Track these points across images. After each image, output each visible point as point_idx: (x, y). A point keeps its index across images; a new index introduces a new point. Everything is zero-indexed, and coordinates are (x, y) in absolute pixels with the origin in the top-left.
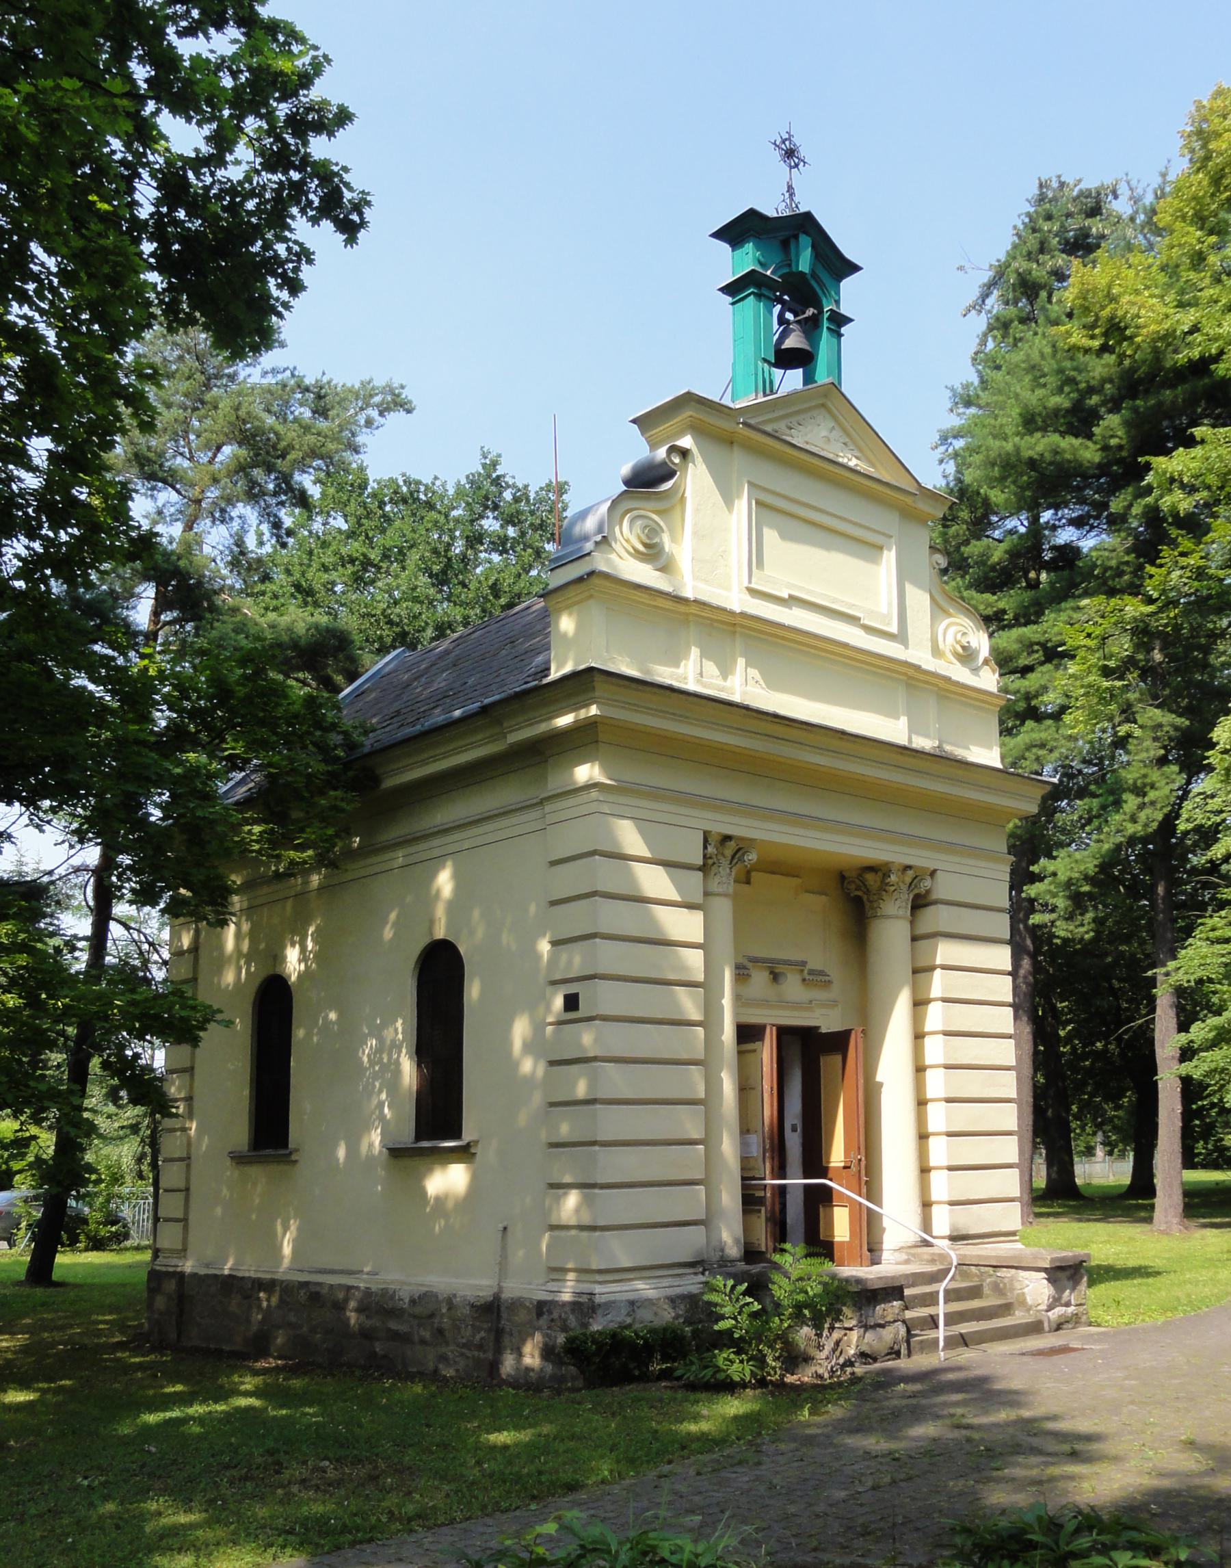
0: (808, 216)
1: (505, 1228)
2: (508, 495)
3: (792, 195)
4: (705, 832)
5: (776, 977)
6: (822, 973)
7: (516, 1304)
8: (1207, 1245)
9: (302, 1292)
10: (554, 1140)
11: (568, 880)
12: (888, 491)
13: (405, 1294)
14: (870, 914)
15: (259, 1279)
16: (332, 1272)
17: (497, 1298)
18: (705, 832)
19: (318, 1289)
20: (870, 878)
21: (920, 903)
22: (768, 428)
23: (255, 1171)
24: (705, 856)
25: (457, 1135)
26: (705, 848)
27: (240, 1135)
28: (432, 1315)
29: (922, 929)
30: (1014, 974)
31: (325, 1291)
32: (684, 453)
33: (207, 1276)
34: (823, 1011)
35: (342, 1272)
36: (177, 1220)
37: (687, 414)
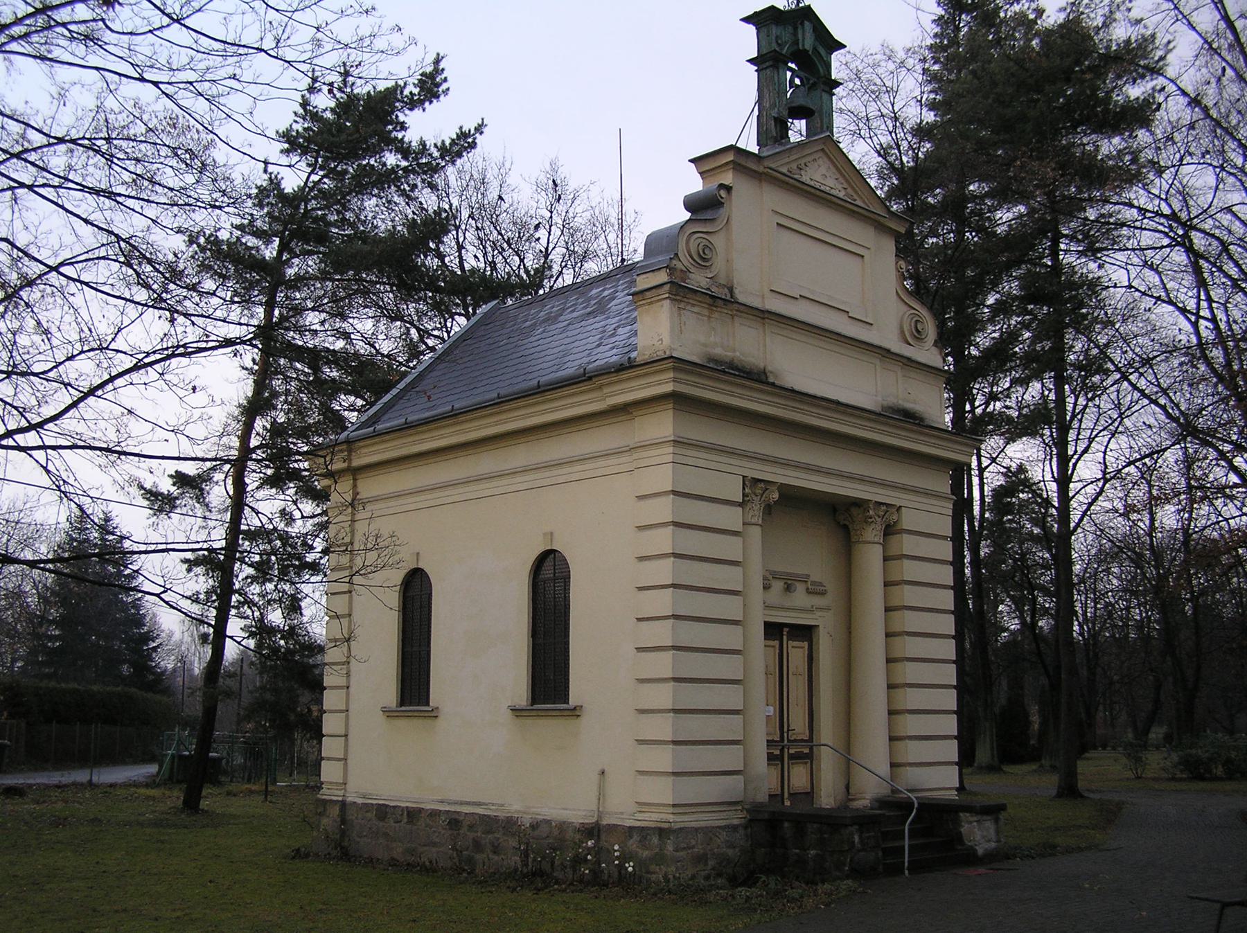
0: (808, 9)
5: (788, 588)
6: (821, 584)
8: (166, 279)
10: (640, 707)
17: (597, 823)
20: (854, 511)
21: (890, 530)
22: (784, 170)
23: (402, 723)
24: (744, 495)
27: (390, 695)
29: (893, 551)
32: (728, 189)
34: (820, 614)
36: (339, 760)
37: (730, 157)
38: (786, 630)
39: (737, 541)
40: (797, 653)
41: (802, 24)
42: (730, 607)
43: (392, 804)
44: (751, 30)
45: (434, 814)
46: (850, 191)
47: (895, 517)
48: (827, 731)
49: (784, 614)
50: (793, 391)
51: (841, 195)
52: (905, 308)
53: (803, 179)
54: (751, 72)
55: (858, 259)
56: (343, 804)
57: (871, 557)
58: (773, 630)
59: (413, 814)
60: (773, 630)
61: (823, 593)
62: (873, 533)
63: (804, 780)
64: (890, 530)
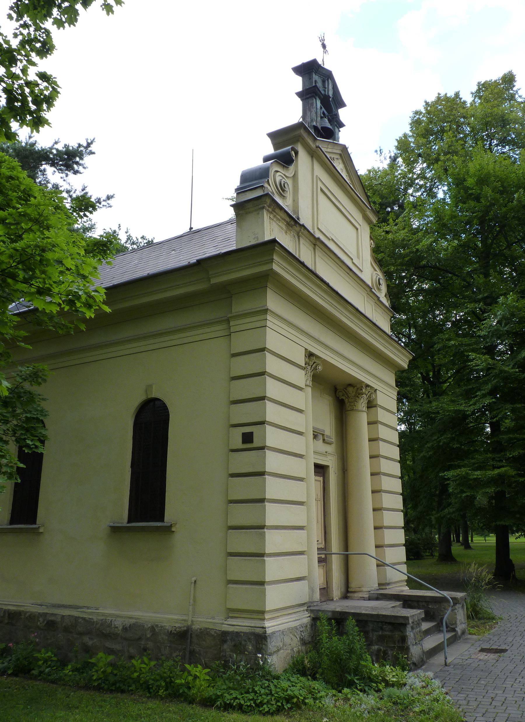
1: (195, 581)
2: (50, 186)
7: (204, 633)
11: (243, 365)
12: (361, 202)
13: (118, 623)
15: (9, 610)
18: (306, 349)
19: (53, 618)
20: (350, 389)
25: (161, 518)
28: (140, 639)
30: (401, 478)
31: (59, 619)
41: (328, 80)
45: (32, 617)
52: (373, 270)
57: (361, 419)
61: (330, 444)
62: (362, 404)
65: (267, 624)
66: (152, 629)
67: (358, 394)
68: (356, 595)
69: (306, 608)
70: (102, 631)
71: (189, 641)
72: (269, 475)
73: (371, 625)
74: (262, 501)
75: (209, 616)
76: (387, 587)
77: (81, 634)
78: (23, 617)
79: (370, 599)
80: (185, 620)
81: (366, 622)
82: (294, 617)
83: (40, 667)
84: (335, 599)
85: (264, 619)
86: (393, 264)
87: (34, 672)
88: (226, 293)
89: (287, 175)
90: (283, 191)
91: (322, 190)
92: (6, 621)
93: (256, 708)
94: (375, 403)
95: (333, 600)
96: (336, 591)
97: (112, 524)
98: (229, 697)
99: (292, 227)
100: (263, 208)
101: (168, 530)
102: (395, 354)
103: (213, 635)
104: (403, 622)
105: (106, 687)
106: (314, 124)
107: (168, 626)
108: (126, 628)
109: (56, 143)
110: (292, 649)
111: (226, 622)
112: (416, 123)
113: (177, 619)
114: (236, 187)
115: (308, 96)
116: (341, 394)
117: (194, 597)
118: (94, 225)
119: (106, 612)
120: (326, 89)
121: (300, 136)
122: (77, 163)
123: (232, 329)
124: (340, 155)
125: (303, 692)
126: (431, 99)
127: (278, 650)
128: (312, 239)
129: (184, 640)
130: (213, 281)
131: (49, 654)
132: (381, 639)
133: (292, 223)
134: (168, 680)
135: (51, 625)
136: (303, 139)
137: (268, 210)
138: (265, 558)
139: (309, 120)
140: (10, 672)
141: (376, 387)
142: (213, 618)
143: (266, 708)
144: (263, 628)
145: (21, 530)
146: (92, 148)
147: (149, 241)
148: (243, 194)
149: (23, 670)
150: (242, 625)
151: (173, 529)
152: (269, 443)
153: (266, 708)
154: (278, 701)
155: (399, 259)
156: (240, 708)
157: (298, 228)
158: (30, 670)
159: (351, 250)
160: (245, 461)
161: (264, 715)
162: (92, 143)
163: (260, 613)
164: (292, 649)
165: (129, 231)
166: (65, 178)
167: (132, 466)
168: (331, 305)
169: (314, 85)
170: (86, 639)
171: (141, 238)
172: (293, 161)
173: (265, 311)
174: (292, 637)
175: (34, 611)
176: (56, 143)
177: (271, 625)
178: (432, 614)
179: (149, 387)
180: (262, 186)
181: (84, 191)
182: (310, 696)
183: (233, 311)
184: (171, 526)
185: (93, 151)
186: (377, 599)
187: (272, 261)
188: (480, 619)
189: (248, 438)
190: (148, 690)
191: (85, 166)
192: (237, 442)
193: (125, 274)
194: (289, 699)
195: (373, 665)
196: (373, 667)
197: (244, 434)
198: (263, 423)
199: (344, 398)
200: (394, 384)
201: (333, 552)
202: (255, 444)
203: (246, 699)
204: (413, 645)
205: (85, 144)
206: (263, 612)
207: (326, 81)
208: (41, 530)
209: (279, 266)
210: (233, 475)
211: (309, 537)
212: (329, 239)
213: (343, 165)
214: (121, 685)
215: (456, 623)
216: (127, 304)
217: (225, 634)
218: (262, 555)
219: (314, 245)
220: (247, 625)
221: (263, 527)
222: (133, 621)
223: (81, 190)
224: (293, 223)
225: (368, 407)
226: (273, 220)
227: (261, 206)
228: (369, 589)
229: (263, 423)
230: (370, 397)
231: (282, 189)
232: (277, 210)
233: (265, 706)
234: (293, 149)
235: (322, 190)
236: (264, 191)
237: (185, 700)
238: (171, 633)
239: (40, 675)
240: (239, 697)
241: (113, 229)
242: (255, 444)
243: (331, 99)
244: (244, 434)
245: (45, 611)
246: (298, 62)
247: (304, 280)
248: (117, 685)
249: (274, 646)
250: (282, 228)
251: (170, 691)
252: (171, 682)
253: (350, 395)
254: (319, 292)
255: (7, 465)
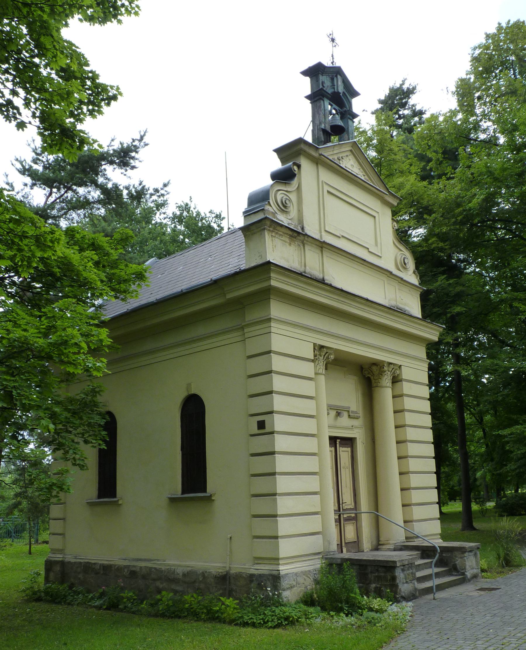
1: (231, 538)
3: (333, 58)
4: (314, 344)
5: (338, 414)
7: (238, 576)
9: (126, 570)
13: (180, 571)
14: (375, 385)
15: (103, 564)
16: (140, 560)
18: (314, 344)
19: (134, 569)
20: (374, 368)
22: (331, 158)
25: (205, 491)
26: (314, 351)
28: (194, 582)
31: (138, 570)
33: (75, 563)
35: (145, 560)
36: (60, 534)
38: (338, 441)
39: (312, 383)
40: (344, 453)
41: (336, 76)
42: (309, 426)
43: (93, 562)
44: (308, 79)
45: (120, 569)
46: (366, 177)
47: (398, 372)
48: (365, 504)
49: (346, 431)
50: (342, 290)
51: (363, 178)
52: (397, 250)
53: (341, 165)
54: (308, 105)
55: (372, 219)
56: (62, 563)
57: (385, 394)
58: (333, 440)
59: (107, 569)
60: (333, 440)
61: (357, 418)
62: (386, 380)
63: (353, 534)
64: (396, 380)
65: (281, 568)
66: (203, 574)
67: (381, 373)
68: (384, 547)
69: (321, 556)
70: (168, 578)
71: (228, 582)
72: (278, 454)
73: (369, 569)
74: (274, 474)
75: (242, 564)
76: (415, 540)
77: (154, 580)
78: (113, 569)
79: (395, 550)
80: (225, 567)
81: (366, 566)
82: (310, 562)
83: (125, 603)
84: (365, 551)
85: (279, 564)
86: (446, 225)
87: (120, 607)
88: (241, 304)
89: (289, 190)
90: (285, 207)
91: (329, 192)
92: (102, 572)
93: (264, 624)
94: (400, 378)
95: (363, 551)
96: (367, 544)
97: (170, 496)
98: (247, 618)
99: (295, 238)
100: (264, 229)
101: (209, 499)
102: (420, 330)
103: (244, 577)
104: (393, 565)
105: (168, 615)
106: (323, 126)
107: (214, 571)
108: (185, 574)
109: (113, 140)
110: (306, 587)
111: (253, 567)
112: (476, 60)
113: (220, 567)
114: (244, 210)
115: (316, 99)
116: (366, 372)
117: (231, 550)
118: (167, 200)
119: (171, 563)
120: (336, 87)
121: (301, 150)
122: (133, 158)
123: (247, 335)
124: (351, 151)
125: (299, 614)
126: (493, 30)
127: (292, 587)
128: (318, 243)
129: (225, 582)
130: (229, 296)
131: (131, 594)
132: (379, 578)
133: (295, 234)
134: (209, 608)
135: (133, 574)
136: (305, 151)
137: (269, 230)
138: (278, 519)
139: (318, 122)
140: (104, 607)
141: (400, 363)
142: (244, 565)
143: (270, 624)
144: (278, 570)
145: (106, 503)
146: (145, 140)
147: (217, 215)
148: (248, 217)
149: (113, 606)
150: (264, 569)
151: (213, 498)
152: (277, 429)
153: (270, 624)
154: (279, 620)
155: (453, 218)
156: (254, 625)
157: (302, 238)
158: (118, 606)
159: (368, 241)
160: (260, 444)
161: (269, 628)
162: (144, 135)
163: (276, 560)
164: (306, 587)
165: (197, 206)
166: (125, 173)
167: (182, 450)
168: (338, 301)
169: (321, 87)
170: (158, 584)
171: (210, 212)
172: (295, 175)
173: (269, 320)
174: (306, 578)
175: (121, 564)
176: (113, 140)
177: (284, 569)
178: (445, 561)
179: (189, 385)
180: (263, 209)
181: (142, 186)
182: (304, 616)
183: (246, 320)
184: (211, 496)
185: (147, 143)
186: (401, 550)
187: (269, 278)
188: (510, 566)
189: (261, 425)
190: (193, 615)
191: (140, 160)
192: (255, 429)
193: (170, 283)
194: (287, 619)
195: (363, 597)
196: (362, 599)
197: (258, 422)
198: (271, 412)
199: (369, 376)
200: (424, 356)
201: (362, 511)
202: (267, 430)
203: (258, 619)
204: (403, 583)
205: (139, 138)
206: (278, 559)
207: (335, 79)
208: (120, 502)
209: (276, 281)
210: (253, 455)
211: (323, 502)
212: (339, 237)
213: (354, 160)
214: (179, 613)
215: (465, 569)
216: (166, 318)
217: (252, 576)
218: (275, 516)
219: (322, 247)
220: (267, 568)
221: (275, 494)
222: (189, 569)
223: (138, 185)
224: (296, 235)
225: (393, 382)
226: (275, 237)
227: (262, 228)
228: (395, 542)
229: (271, 412)
230: (394, 373)
231: (284, 207)
232: (278, 228)
233: (270, 623)
234: (294, 164)
235: (329, 192)
236: (264, 214)
237: (220, 622)
238: (216, 577)
239: (125, 609)
240: (254, 617)
241: (185, 202)
242: (267, 430)
243: (341, 94)
244: (258, 422)
245: (128, 564)
246: (305, 67)
247: (304, 286)
248: (175, 613)
249: (287, 584)
250: (285, 241)
251: (210, 616)
252: (211, 609)
253: (374, 373)
254: (324, 293)
255: (79, 459)
